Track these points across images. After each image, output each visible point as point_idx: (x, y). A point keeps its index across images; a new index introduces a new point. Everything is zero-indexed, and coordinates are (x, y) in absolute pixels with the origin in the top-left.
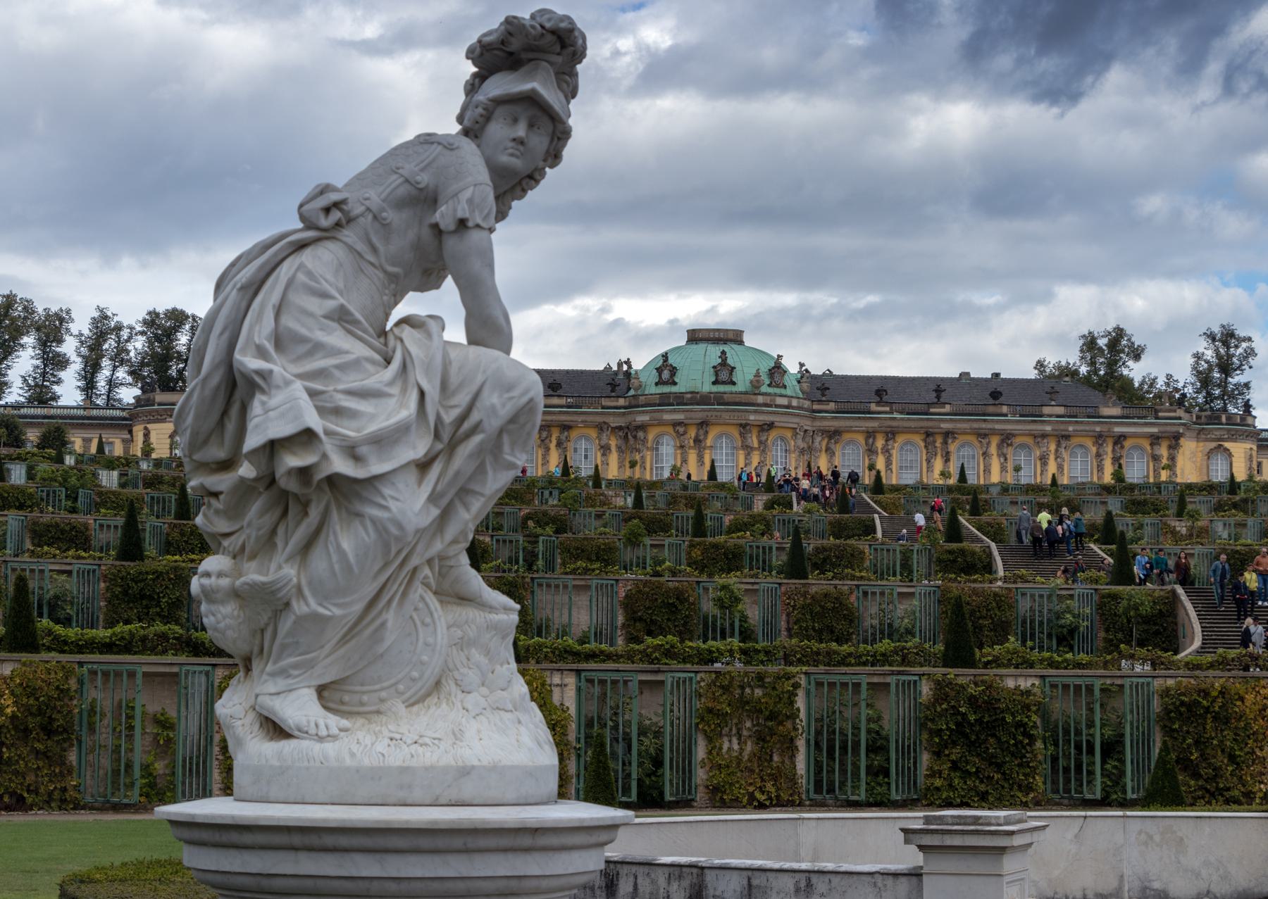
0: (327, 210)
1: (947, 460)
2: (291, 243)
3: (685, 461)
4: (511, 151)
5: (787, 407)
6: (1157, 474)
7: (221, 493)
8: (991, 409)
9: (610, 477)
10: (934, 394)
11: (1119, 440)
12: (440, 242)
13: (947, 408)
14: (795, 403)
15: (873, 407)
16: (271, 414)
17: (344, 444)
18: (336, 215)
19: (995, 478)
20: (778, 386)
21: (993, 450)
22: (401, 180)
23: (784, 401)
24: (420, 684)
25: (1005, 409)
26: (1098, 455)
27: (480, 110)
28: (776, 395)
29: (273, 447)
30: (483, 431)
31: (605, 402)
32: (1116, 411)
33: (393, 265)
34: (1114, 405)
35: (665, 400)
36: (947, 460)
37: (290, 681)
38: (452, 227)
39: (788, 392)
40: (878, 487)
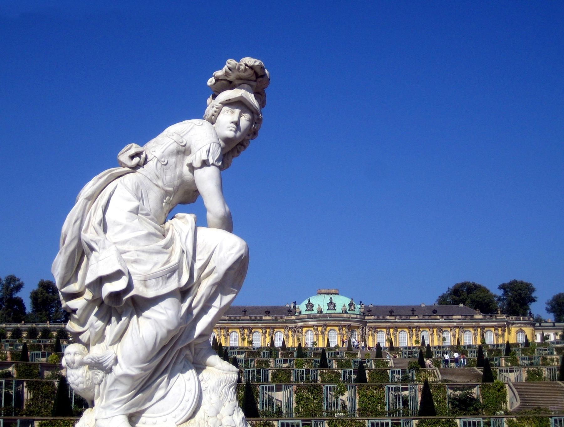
0: (132, 157)
1: (417, 337)
2: (111, 175)
3: (318, 340)
4: (231, 128)
5: (356, 318)
6: (497, 340)
7: (77, 310)
8: (433, 317)
9: (289, 346)
10: (411, 312)
11: (483, 328)
12: (193, 174)
13: (417, 317)
14: (358, 316)
15: (388, 317)
16: (99, 262)
17: (140, 279)
18: (136, 160)
19: (436, 344)
20: (352, 310)
21: (435, 333)
22: (173, 141)
23: (355, 316)
25: (438, 317)
26: (475, 334)
27: (215, 109)
29: (101, 281)
32: (480, 317)
33: (169, 186)
34: (480, 314)
35: (309, 317)
36: (417, 337)
37: (113, 411)
38: (199, 165)
39: (356, 313)
40: (392, 348)
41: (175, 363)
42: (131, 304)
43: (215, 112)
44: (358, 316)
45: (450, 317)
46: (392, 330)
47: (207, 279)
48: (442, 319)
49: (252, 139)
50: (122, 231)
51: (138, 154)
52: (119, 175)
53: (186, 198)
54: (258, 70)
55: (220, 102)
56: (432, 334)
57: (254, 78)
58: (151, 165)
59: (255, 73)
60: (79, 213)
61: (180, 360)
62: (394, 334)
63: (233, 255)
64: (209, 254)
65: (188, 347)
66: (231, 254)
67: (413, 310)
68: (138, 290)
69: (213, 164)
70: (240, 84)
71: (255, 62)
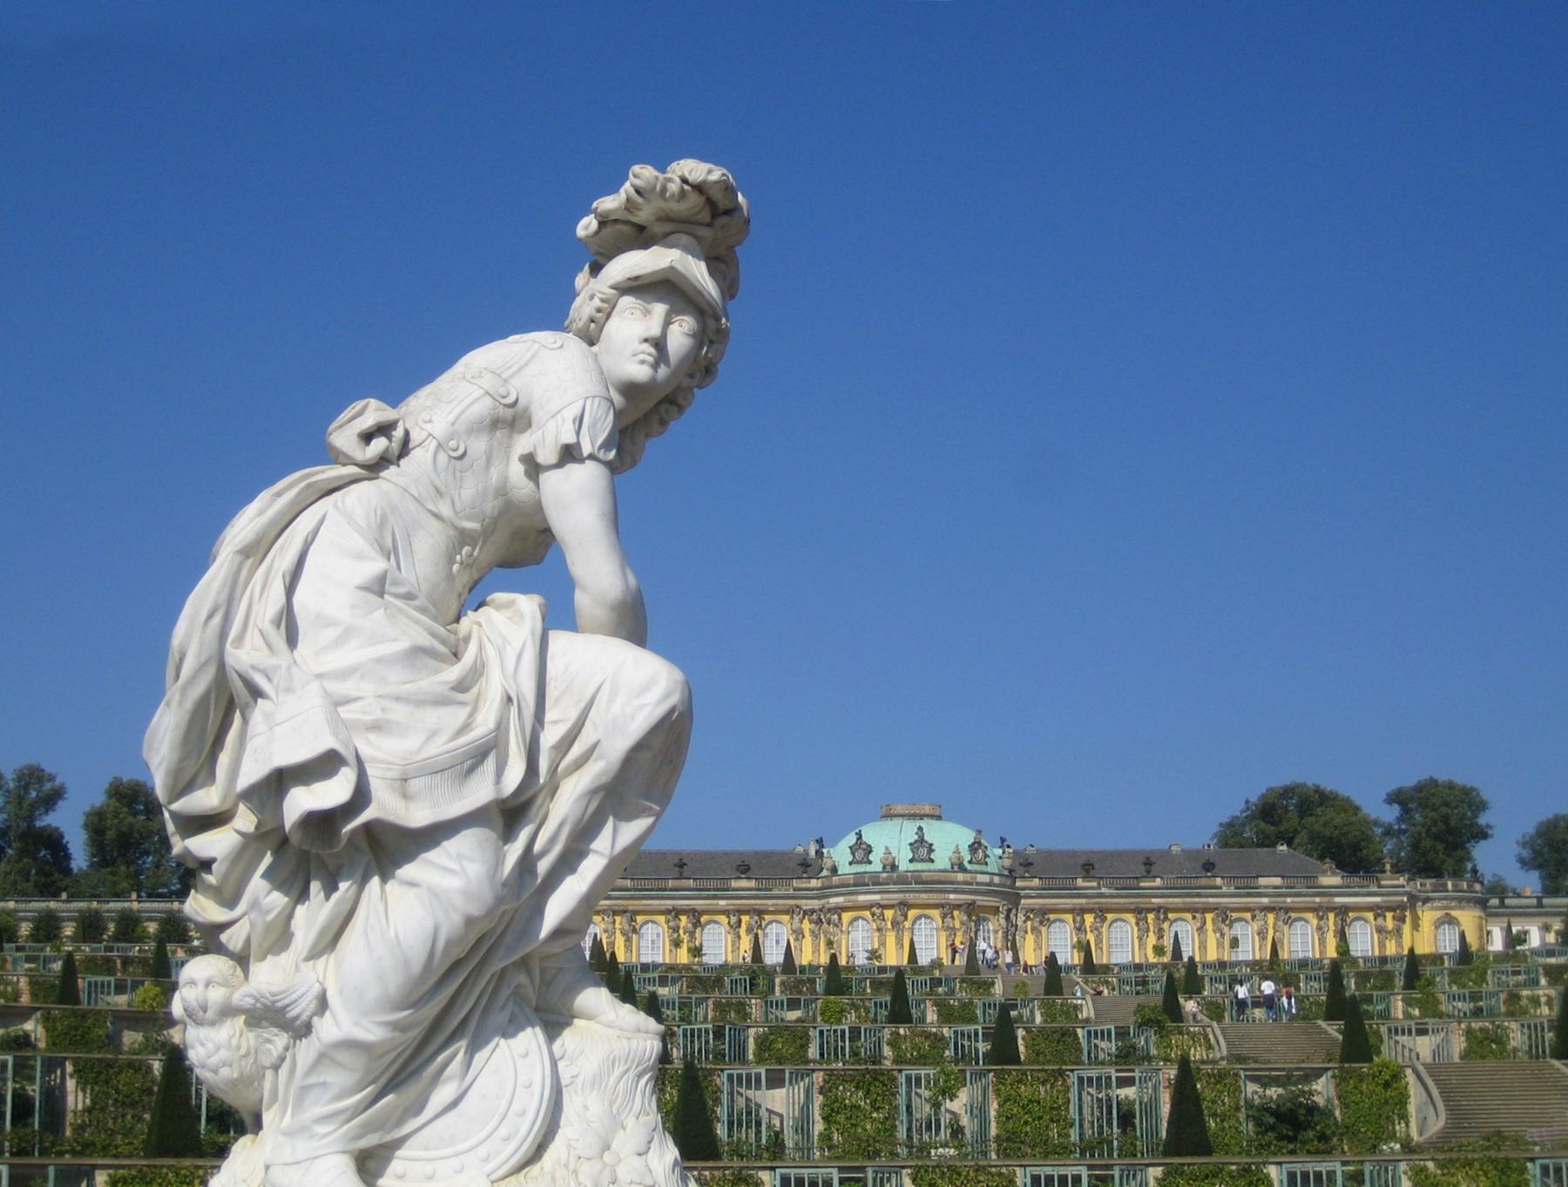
0: (367, 437)
1: (1160, 937)
2: (309, 486)
3: (883, 944)
4: (642, 357)
6: (1382, 945)
7: (213, 860)
8: (1204, 881)
9: (804, 963)
10: (1143, 868)
11: (1342, 911)
13: (1158, 882)
14: (996, 880)
15: (1080, 882)
16: (277, 729)
18: (379, 444)
19: (1212, 955)
20: (979, 863)
21: (1209, 926)
23: (986, 878)
24: (512, 1146)
26: (1319, 928)
27: (597, 302)
28: (977, 872)
29: (281, 781)
30: (601, 757)
31: (795, 883)
32: (1335, 880)
33: (469, 518)
34: (1334, 874)
35: (860, 882)
36: (1160, 937)
38: (553, 459)
39: (989, 869)
40: (1089, 967)
41: (486, 1011)
42: (364, 845)
43: (599, 310)
44: (996, 880)
45: (1251, 882)
46: (1089, 919)
47: (575, 776)
48: (1229, 886)
49: (700, 387)
50: (339, 642)
51: (384, 429)
52: (336, 484)
53: (518, 550)
54: (717, 195)
55: (611, 282)
56: (1201, 929)
57: (705, 216)
58: (419, 457)
59: (710, 202)
60: (218, 593)
61: (501, 1001)
62: (1096, 930)
63: (648, 709)
64: (582, 705)
65: (524, 964)
66: (642, 707)
67: (1148, 863)
68: (385, 806)
69: (592, 457)
70: (667, 235)
71: (710, 172)
